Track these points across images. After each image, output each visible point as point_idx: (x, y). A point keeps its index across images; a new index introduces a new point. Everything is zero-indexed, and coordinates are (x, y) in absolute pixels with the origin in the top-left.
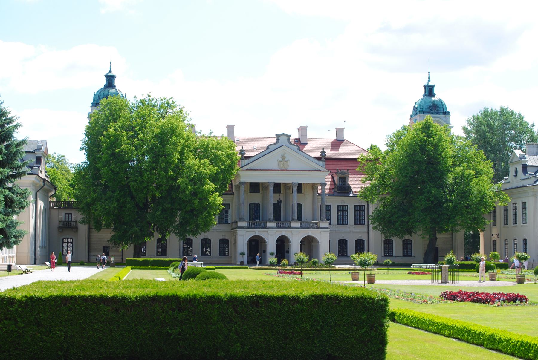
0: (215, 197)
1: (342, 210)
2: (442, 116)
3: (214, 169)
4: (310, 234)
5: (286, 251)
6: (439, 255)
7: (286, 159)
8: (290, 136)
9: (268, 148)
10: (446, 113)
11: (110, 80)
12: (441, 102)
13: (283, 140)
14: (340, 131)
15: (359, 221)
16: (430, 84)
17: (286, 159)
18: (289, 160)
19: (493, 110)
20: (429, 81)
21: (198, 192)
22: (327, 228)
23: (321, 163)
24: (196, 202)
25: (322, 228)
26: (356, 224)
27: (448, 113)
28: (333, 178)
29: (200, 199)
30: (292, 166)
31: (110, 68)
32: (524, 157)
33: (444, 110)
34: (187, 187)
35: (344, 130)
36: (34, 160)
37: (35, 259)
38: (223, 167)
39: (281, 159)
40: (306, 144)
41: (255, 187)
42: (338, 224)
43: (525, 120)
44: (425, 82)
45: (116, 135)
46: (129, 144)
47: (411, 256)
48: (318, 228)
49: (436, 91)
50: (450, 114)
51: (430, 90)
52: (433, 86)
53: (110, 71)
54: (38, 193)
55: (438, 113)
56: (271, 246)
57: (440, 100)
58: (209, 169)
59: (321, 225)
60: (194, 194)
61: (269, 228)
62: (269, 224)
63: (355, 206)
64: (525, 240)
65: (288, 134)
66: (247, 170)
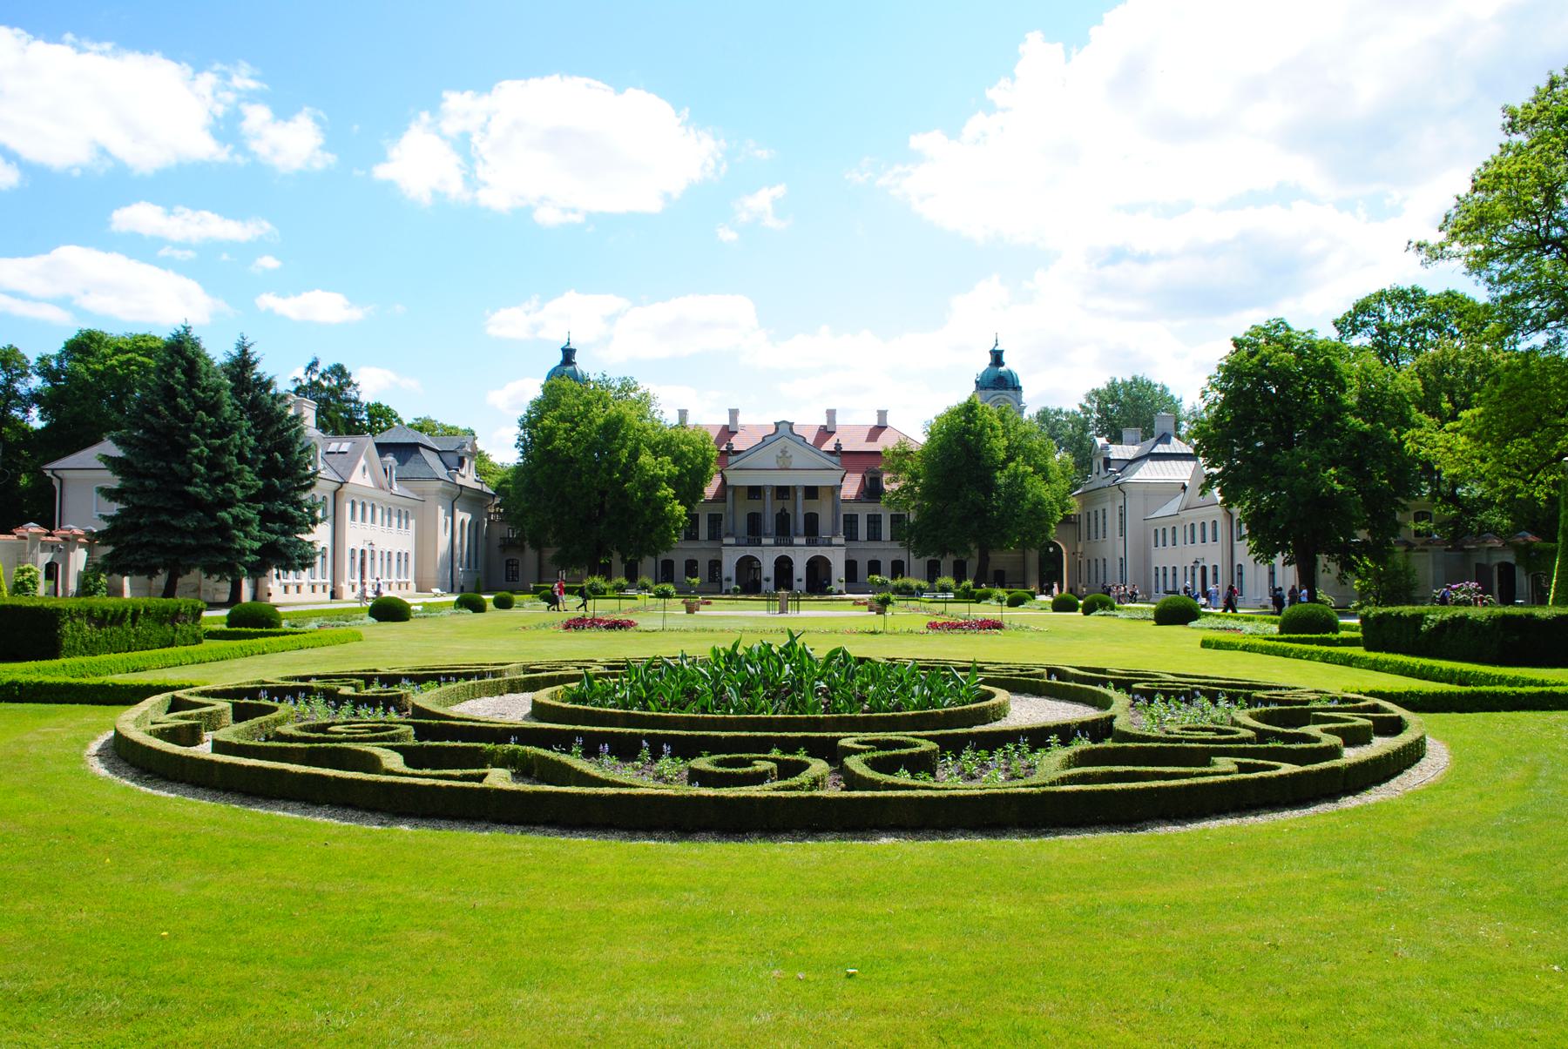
0: (673, 507)
1: (874, 521)
2: (1011, 392)
3: (676, 470)
4: (748, 554)
9: (763, 440)
10: (1018, 389)
12: (1010, 372)
14: (882, 414)
15: (874, 535)
16: (997, 349)
17: (788, 455)
20: (997, 345)
22: (842, 546)
23: (834, 459)
24: (647, 512)
25: (835, 545)
27: (1020, 388)
28: (864, 477)
29: (653, 509)
32: (1107, 448)
36: (456, 461)
37: (453, 586)
38: (690, 466)
39: (780, 455)
41: (755, 492)
42: (868, 539)
43: (1171, 393)
46: (565, 439)
47: (857, 540)
49: (1005, 358)
51: (997, 358)
52: (1001, 352)
53: (569, 343)
55: (1006, 389)
56: (768, 570)
58: (667, 467)
59: (834, 541)
60: (646, 501)
62: (796, 541)
64: (1104, 560)
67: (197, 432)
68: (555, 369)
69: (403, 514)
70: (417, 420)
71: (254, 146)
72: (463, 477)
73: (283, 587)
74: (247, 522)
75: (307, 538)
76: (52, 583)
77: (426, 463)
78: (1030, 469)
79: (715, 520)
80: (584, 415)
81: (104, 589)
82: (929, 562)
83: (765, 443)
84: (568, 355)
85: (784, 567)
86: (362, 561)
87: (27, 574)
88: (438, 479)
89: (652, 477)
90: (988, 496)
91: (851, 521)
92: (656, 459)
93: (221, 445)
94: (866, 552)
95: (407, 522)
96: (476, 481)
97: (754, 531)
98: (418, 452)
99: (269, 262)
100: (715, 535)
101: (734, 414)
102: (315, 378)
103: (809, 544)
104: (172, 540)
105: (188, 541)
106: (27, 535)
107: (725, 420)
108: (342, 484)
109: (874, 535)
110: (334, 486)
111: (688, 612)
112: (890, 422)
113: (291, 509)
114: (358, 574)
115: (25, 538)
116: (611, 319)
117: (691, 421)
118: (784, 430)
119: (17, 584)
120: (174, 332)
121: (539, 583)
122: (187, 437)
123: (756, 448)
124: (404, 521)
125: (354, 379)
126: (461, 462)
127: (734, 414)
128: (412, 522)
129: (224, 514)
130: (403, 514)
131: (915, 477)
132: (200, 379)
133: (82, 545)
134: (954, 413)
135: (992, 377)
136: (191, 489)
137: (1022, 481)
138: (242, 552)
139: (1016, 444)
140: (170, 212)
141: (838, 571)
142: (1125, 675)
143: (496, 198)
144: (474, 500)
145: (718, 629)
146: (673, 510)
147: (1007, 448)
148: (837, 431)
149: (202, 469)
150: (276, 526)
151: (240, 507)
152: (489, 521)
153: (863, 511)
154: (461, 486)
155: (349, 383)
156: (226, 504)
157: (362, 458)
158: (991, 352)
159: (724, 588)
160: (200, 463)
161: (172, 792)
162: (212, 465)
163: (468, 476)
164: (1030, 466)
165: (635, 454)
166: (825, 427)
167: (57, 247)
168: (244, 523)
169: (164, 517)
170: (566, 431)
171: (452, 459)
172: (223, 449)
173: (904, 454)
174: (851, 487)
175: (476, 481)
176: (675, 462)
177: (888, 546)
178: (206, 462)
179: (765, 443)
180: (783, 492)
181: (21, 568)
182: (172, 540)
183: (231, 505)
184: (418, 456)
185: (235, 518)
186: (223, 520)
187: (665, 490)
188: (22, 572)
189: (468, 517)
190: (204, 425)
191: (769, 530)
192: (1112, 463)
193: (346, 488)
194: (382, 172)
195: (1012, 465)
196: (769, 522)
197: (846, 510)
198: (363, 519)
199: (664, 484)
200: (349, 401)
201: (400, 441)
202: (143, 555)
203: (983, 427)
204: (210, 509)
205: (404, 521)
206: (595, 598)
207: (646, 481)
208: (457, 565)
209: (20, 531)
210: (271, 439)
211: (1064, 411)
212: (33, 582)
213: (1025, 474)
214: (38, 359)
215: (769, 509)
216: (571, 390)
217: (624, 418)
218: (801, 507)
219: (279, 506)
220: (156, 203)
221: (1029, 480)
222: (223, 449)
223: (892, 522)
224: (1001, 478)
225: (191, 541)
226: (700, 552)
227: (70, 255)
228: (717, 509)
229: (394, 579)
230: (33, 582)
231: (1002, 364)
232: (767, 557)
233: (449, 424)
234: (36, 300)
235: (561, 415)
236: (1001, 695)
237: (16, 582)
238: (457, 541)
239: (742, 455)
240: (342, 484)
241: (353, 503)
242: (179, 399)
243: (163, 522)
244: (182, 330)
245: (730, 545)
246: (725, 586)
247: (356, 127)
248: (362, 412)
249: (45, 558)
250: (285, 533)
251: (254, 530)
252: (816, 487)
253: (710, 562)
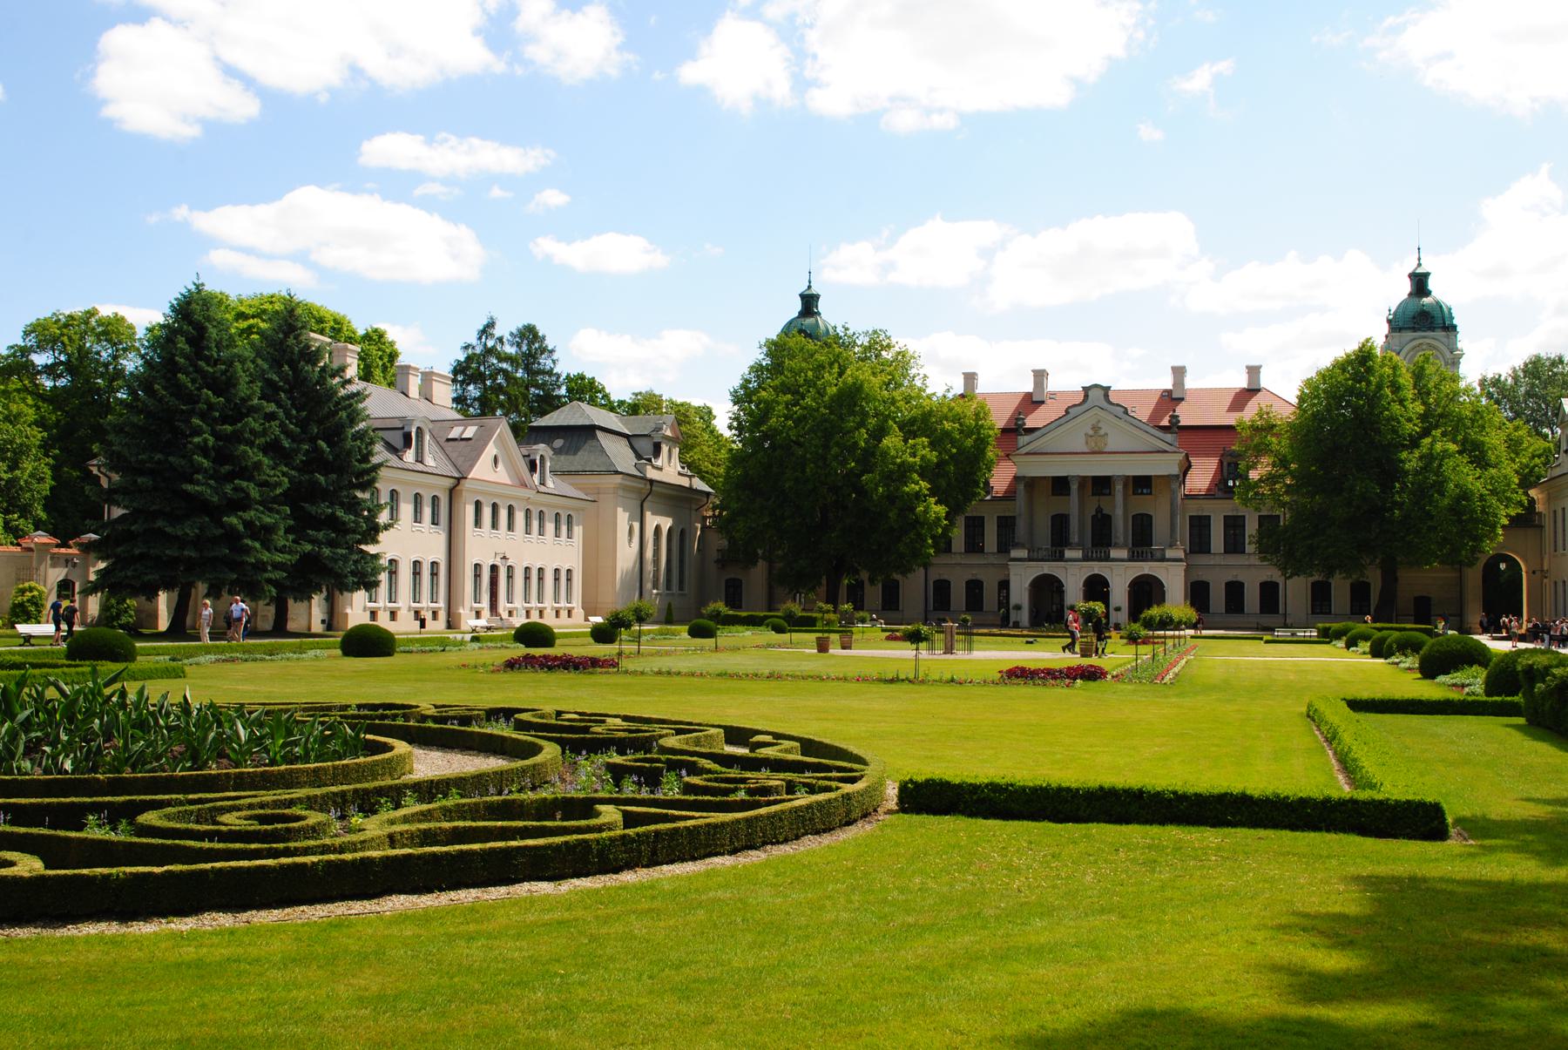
1: (1234, 525)
2: (1439, 334)
3: (933, 456)
4: (1046, 571)
6: (1432, 613)
7: (1102, 432)
8: (1109, 387)
9: (1067, 412)
11: (809, 303)
12: (1439, 305)
13: (1095, 395)
15: (1234, 544)
16: (1419, 271)
17: (1102, 432)
18: (1106, 434)
19: (515, 332)
21: (897, 497)
22: (1180, 560)
23: (1169, 437)
25: (1169, 560)
26: (967, 551)
27: (1454, 328)
28: (1221, 462)
30: (1111, 447)
31: (810, 282)
33: (1444, 323)
34: (876, 490)
35: (1261, 370)
38: (954, 451)
39: (1091, 432)
40: (1182, 399)
41: (1060, 485)
42: (1226, 552)
44: (803, 288)
48: (1163, 559)
49: (1432, 284)
50: (1458, 329)
51: (1420, 283)
52: (1426, 275)
53: (809, 287)
54: (645, 505)
55: (1432, 329)
57: (1437, 303)
58: (923, 450)
59: (1169, 554)
60: (891, 498)
61: (1067, 561)
62: (1114, 553)
63: (1225, 517)
64: (1564, 582)
65: (1105, 385)
66: (1027, 454)
67: (203, 416)
68: (790, 322)
69: (564, 519)
70: (636, 395)
71: (531, 51)
73: (368, 613)
74: (269, 529)
75: (371, 549)
77: (603, 450)
78: (1453, 447)
80: (810, 383)
81: (132, 613)
82: (1314, 584)
83: (1068, 417)
84: (809, 303)
85: (1096, 588)
86: (493, 579)
87: (28, 594)
88: (617, 472)
89: (900, 466)
90: (1387, 486)
91: (1200, 526)
92: (906, 441)
93: (234, 432)
94: (1220, 569)
95: (570, 530)
96: (680, 474)
98: (594, 437)
99: (554, 198)
100: (1004, 547)
102: (490, 343)
103: (1133, 558)
104: (167, 552)
105: (186, 553)
106: (32, 546)
108: (458, 480)
110: (449, 483)
111: (820, 651)
112: (1265, 382)
113: (340, 513)
114: (486, 598)
116: (987, 253)
117: (982, 387)
118: (1095, 396)
119: (15, 606)
120: (184, 291)
121: (770, 610)
122: (188, 421)
123: (1057, 423)
124: (564, 528)
125: (549, 343)
128: (578, 530)
129: (234, 520)
130: (564, 519)
131: (1283, 462)
132: (209, 349)
134: (1341, 366)
135: (1410, 313)
136: (189, 487)
137: (1440, 466)
138: (261, 566)
139: (1440, 410)
140: (430, 141)
142: (580, 721)
143: (831, 101)
144: (676, 499)
145: (766, 672)
146: (926, 511)
147: (1424, 417)
148: (1187, 398)
149: (206, 463)
150: (320, 535)
151: (257, 510)
153: (1217, 513)
154: (652, 482)
155: (543, 350)
156: (240, 503)
157: (491, 443)
159: (1012, 619)
160: (206, 456)
161: (1286, 934)
162: (221, 457)
163: (666, 468)
164: (1454, 442)
165: (880, 433)
166: (1169, 392)
167: (293, 189)
168: (264, 534)
169: (160, 523)
170: (787, 404)
171: (645, 446)
172: (237, 437)
173: (1266, 428)
174: (1202, 476)
175: (680, 474)
176: (933, 445)
177: (992, 560)
178: (213, 454)
180: (1102, 485)
181: (21, 586)
182: (167, 552)
183: (245, 508)
184: (594, 443)
185: (248, 524)
186: (233, 528)
187: (917, 483)
188: (23, 591)
189: (666, 523)
190: (211, 407)
191: (1121, 540)
193: (466, 484)
194: (691, 73)
195: (1427, 441)
197: (1194, 509)
199: (915, 476)
200: (543, 372)
201: (572, 423)
202: (135, 570)
203: (1380, 387)
204: (214, 512)
205: (564, 528)
206: (790, 631)
207: (891, 472)
208: (649, 585)
210: (320, 422)
211: (555, 357)
212: (36, 604)
213: (1445, 454)
214: (147, 329)
216: (802, 349)
217: (861, 386)
218: (1119, 509)
219: (324, 509)
220: (412, 131)
221: (1450, 463)
222: (237, 437)
223: (1226, 526)
224: (1411, 461)
225: (190, 553)
226: (983, 569)
227: (307, 197)
229: (548, 603)
230: (36, 604)
231: (1427, 293)
232: (1073, 576)
233: (679, 401)
234: (271, 257)
235: (783, 384)
236: (401, 747)
237: (14, 604)
238: (649, 554)
239: (1037, 434)
240: (458, 480)
241: (478, 505)
242: (179, 375)
243: (159, 528)
244: (193, 288)
247: (653, 20)
248: (559, 387)
250: (332, 544)
251: (281, 539)
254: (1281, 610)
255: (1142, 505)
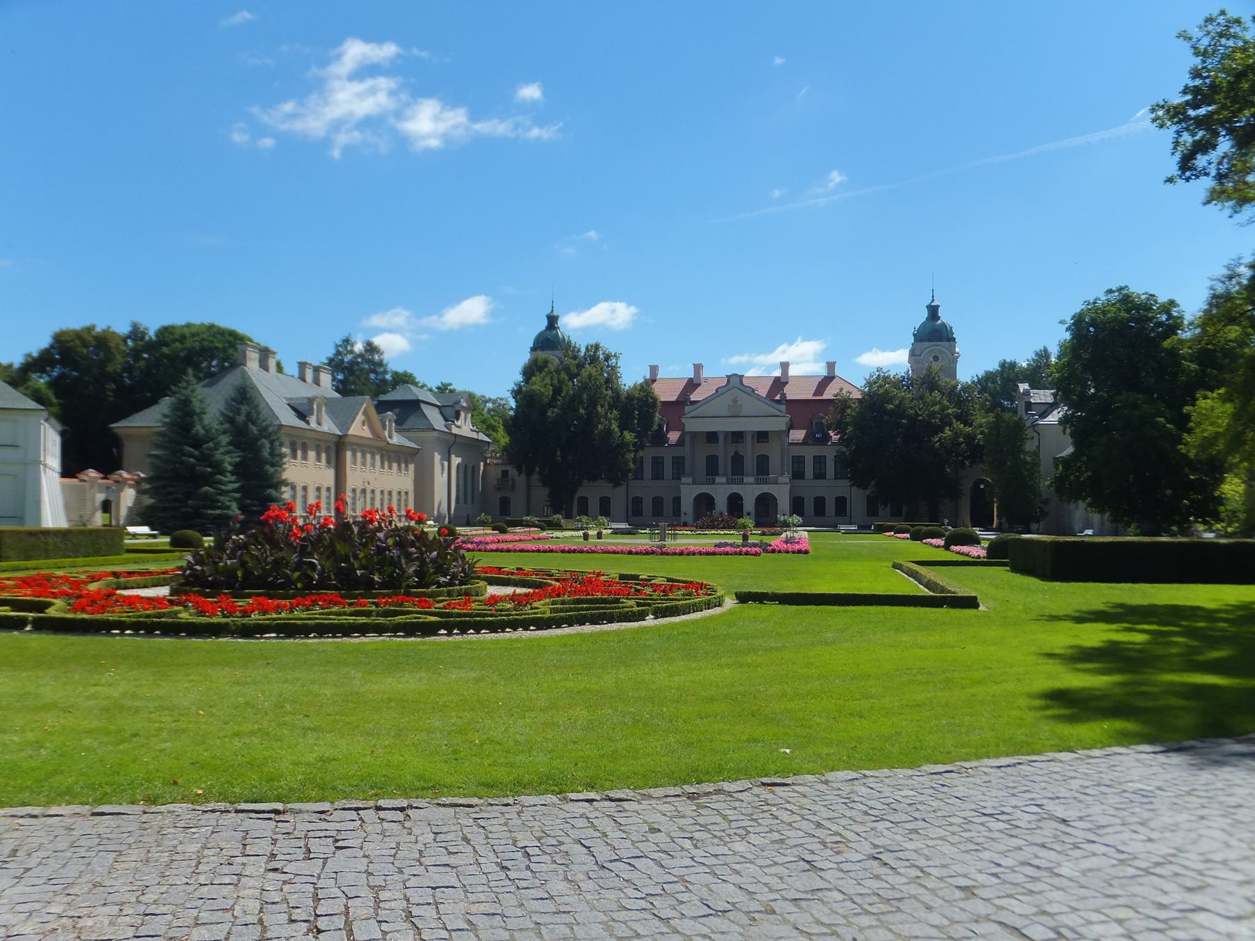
5: (507, 471)
9: (717, 391)
13: (734, 381)
15: (820, 475)
17: (739, 403)
27: (955, 339)
39: (731, 404)
41: (712, 437)
45: (1206, 437)
47: (642, 479)
49: (940, 313)
51: (933, 311)
52: (937, 307)
55: (941, 340)
59: (780, 479)
62: (746, 479)
72: (459, 427)
76: (107, 515)
79: (678, 462)
94: (811, 489)
97: (712, 468)
101: (698, 368)
103: (758, 482)
107: (778, 373)
109: (820, 475)
115: (85, 481)
126: (457, 417)
127: (698, 368)
128: (411, 467)
133: (131, 486)
141: (784, 503)
152: (486, 465)
158: (927, 307)
163: (464, 427)
179: (719, 394)
180: (738, 436)
192: (1033, 406)
196: (724, 463)
198: (364, 464)
209: (82, 476)
215: (723, 452)
218: (749, 453)
228: (679, 452)
239: (699, 404)
245: (750, 484)
246: (683, 518)
249: (100, 497)
252: (767, 432)
253: (674, 499)
254: (848, 514)
255: (762, 449)
